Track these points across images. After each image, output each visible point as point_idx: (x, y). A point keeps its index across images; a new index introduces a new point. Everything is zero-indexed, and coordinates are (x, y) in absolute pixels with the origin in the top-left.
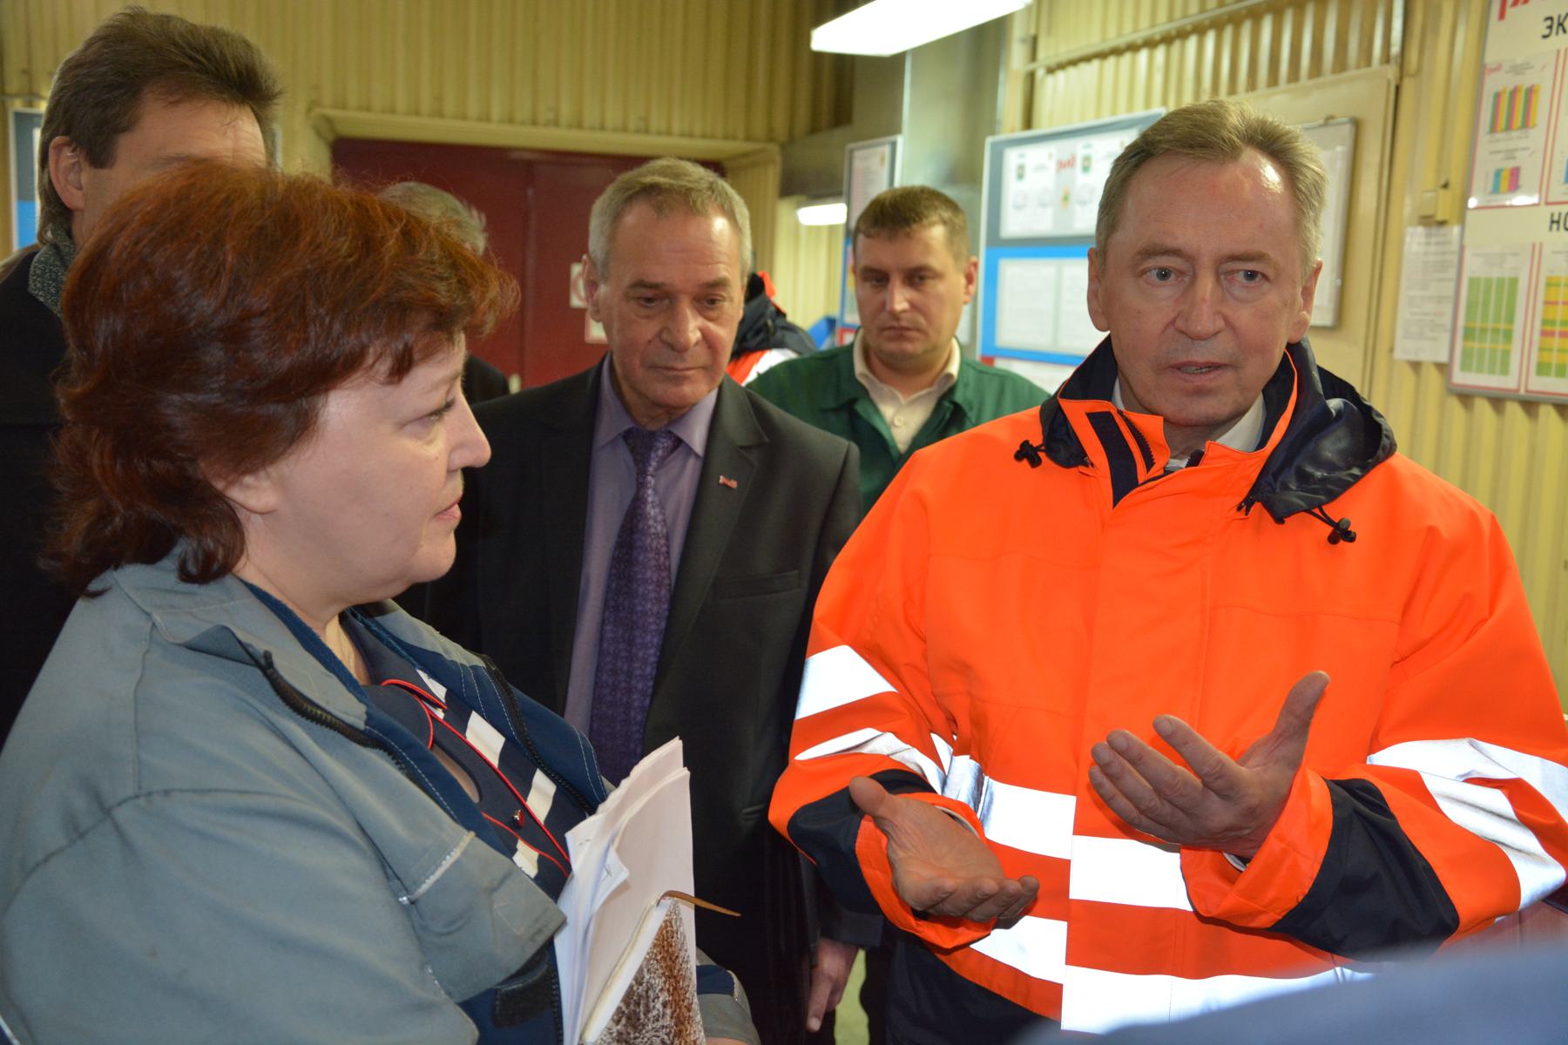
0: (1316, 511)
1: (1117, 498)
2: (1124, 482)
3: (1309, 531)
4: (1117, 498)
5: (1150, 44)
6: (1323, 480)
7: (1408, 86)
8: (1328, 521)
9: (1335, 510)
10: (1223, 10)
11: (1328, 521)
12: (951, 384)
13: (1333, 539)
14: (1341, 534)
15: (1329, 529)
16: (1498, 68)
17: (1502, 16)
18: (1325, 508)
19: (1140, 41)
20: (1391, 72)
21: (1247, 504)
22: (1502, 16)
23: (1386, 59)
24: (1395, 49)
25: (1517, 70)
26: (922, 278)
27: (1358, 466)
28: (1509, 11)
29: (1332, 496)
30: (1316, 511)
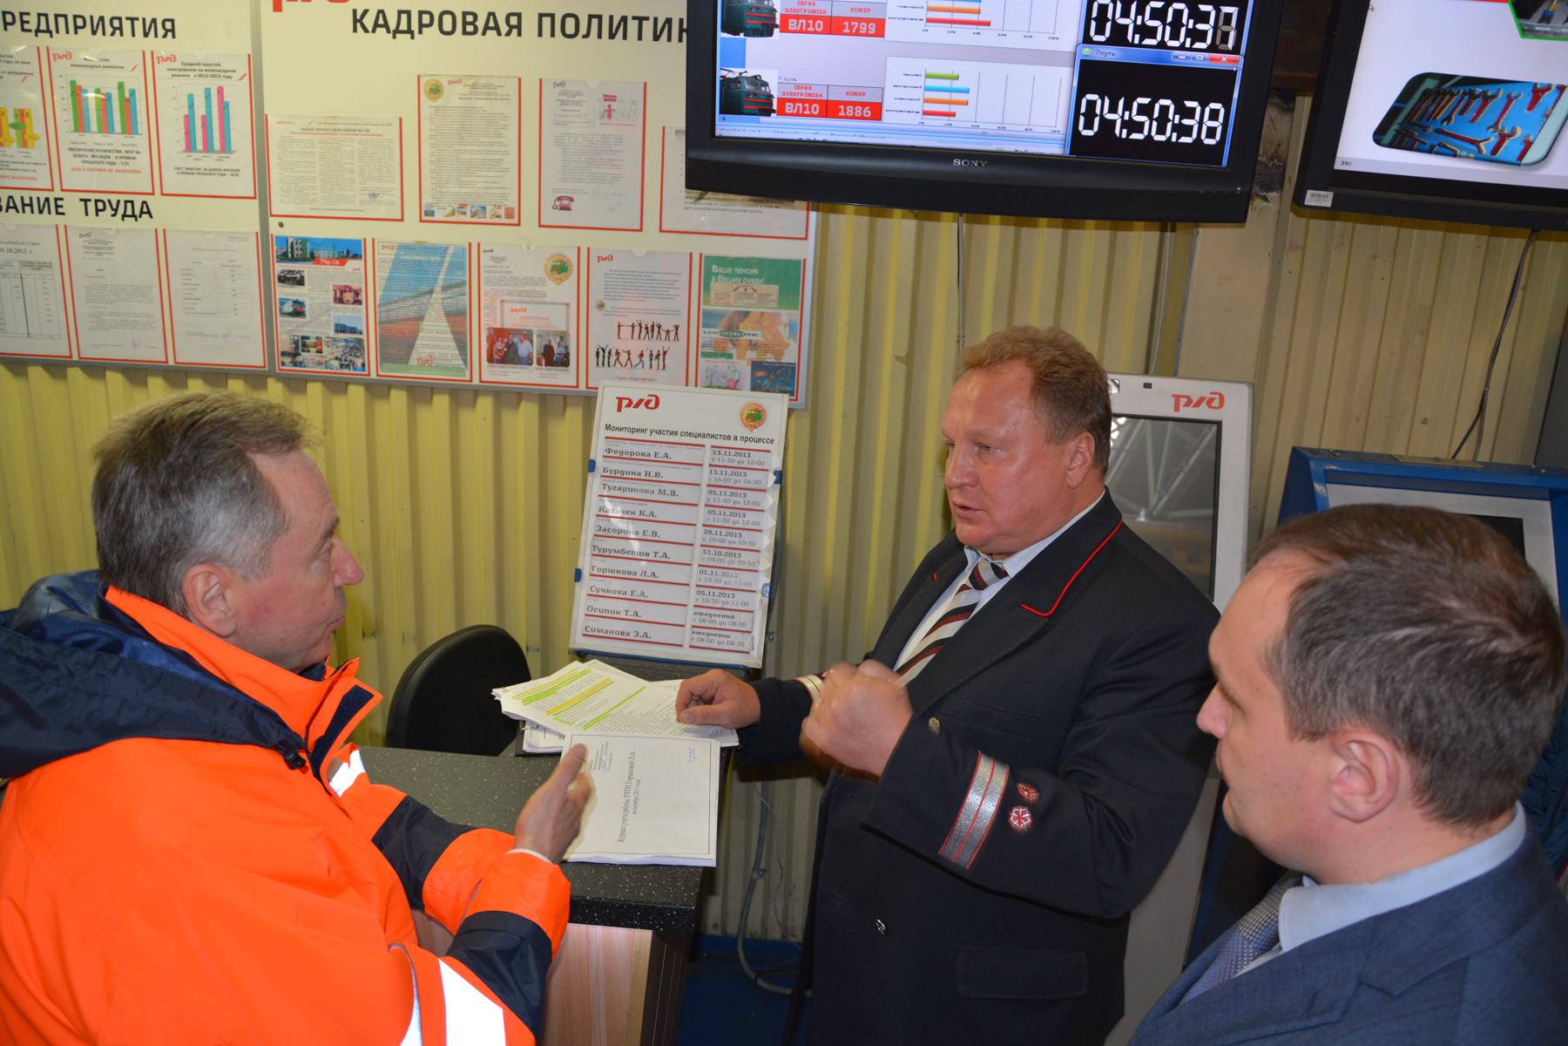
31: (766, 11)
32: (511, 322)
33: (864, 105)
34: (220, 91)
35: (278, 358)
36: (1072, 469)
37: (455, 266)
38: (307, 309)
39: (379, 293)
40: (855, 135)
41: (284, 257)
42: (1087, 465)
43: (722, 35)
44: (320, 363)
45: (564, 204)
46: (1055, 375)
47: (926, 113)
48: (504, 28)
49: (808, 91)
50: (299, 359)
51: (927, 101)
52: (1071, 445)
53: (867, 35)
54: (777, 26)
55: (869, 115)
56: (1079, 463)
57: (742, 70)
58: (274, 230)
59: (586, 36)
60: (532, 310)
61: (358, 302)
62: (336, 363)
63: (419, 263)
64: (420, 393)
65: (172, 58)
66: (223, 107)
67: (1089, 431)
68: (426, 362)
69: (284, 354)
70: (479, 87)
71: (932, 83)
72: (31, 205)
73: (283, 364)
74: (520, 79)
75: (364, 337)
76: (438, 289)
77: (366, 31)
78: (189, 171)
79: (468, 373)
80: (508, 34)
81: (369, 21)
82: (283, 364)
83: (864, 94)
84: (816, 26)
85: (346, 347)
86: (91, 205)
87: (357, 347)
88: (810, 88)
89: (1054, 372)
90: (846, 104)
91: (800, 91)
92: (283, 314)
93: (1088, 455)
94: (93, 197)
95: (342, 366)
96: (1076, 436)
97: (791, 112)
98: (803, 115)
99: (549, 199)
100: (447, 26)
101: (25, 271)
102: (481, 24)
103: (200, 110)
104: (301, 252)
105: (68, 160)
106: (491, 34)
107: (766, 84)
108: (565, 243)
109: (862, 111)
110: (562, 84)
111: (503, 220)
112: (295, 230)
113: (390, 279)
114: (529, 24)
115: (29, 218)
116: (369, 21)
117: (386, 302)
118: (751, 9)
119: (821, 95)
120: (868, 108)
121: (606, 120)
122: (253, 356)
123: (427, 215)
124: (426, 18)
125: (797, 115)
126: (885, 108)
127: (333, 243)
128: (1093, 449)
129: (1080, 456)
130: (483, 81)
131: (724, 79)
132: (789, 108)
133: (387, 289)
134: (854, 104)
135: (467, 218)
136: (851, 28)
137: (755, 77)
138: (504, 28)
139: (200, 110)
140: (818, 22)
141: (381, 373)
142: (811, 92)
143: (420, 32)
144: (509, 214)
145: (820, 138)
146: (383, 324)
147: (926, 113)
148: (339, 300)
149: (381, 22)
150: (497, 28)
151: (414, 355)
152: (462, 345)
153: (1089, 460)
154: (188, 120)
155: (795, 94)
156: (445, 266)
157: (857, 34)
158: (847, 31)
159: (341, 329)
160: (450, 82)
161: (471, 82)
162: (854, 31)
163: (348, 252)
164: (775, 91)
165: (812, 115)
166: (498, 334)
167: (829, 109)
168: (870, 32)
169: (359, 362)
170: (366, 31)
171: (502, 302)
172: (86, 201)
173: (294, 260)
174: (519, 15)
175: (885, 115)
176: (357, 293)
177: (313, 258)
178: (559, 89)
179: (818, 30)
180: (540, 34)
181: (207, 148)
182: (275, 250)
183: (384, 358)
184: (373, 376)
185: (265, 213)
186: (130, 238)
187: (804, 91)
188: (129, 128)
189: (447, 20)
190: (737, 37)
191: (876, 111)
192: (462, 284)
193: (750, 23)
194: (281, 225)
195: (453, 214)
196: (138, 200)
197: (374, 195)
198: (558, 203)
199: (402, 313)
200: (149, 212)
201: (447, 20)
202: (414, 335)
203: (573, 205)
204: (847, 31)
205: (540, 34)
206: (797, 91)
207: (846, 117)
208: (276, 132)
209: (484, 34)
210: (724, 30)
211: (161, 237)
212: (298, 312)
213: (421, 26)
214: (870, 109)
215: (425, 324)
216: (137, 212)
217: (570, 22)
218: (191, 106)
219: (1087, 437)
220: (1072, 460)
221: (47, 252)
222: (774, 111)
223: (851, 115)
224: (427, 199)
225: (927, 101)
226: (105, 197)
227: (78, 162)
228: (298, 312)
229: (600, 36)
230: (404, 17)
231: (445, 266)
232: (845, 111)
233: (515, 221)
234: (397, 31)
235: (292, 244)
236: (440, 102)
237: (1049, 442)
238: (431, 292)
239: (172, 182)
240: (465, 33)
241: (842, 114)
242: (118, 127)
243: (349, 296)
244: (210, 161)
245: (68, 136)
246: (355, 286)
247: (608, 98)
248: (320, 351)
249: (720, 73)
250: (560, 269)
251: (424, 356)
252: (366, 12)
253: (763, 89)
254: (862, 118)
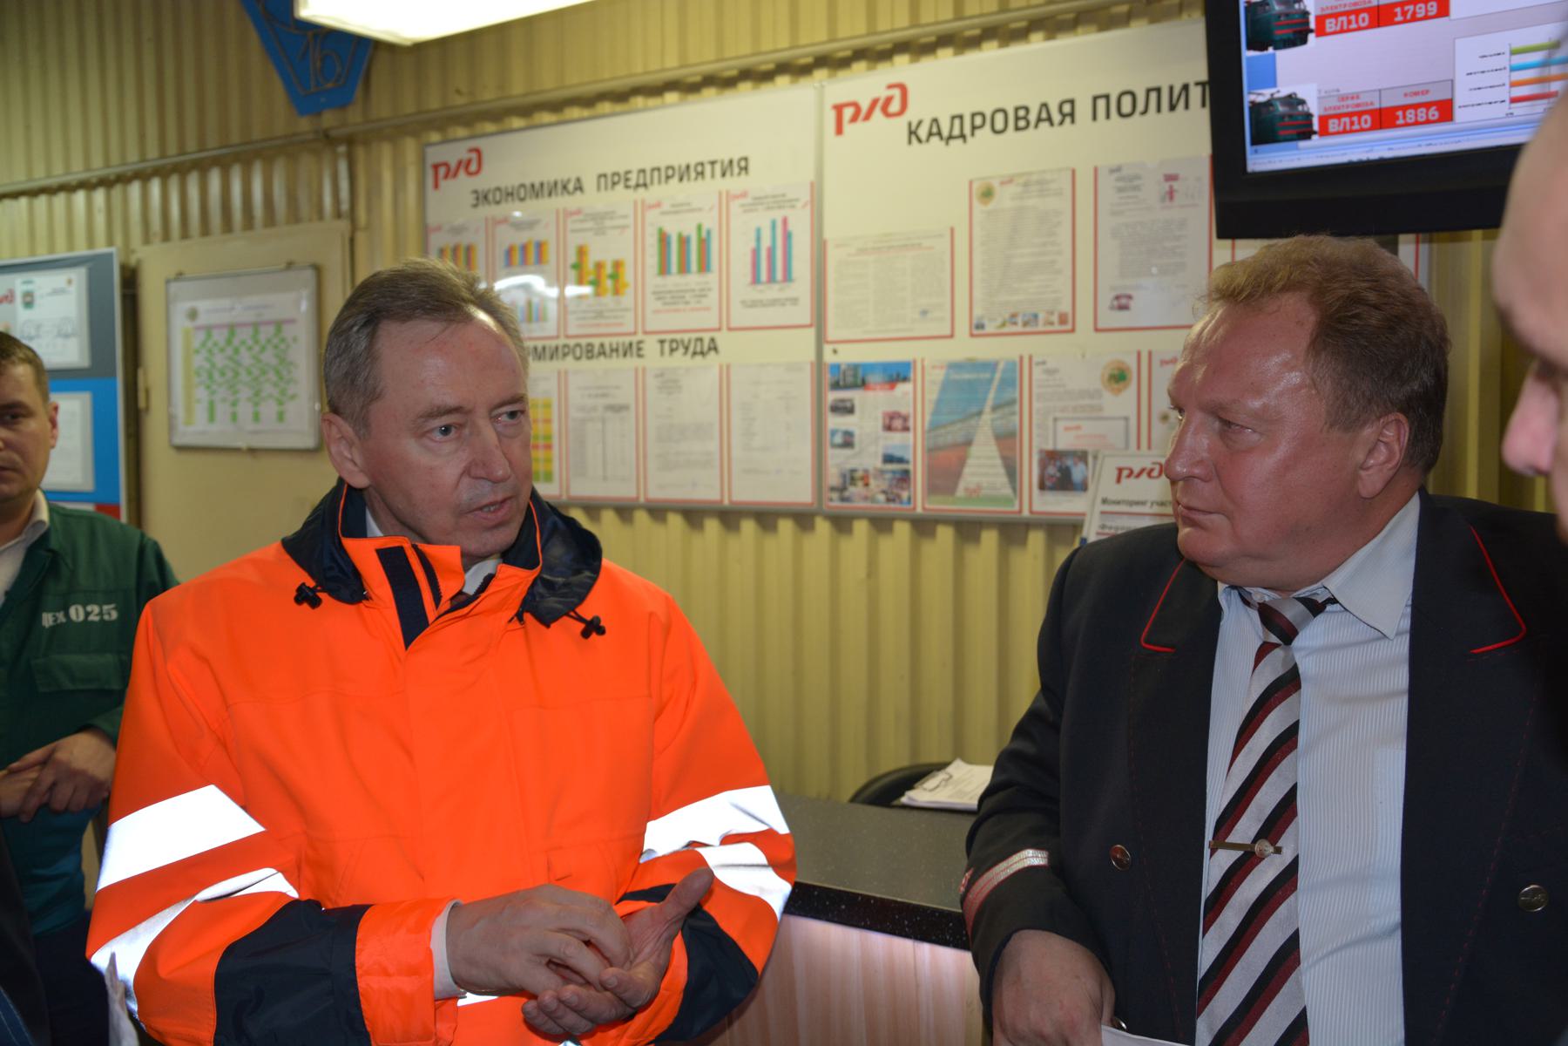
0: (572, 614)
1: (408, 640)
2: (413, 623)
3: (567, 628)
4: (408, 640)
5: (87, 186)
6: (565, 585)
7: (361, 238)
8: (580, 619)
9: (588, 610)
10: (182, 158)
11: (580, 619)
12: (43, 530)
13: (586, 634)
14: (593, 628)
15: (582, 626)
16: (439, 228)
17: (436, 186)
18: (578, 610)
19: (94, 180)
20: (344, 225)
21: (519, 617)
22: (436, 186)
23: (338, 215)
24: (345, 207)
25: (457, 230)
26: (15, 417)
27: (587, 569)
28: (442, 183)
29: (582, 598)
30: (572, 614)
31: (1297, 16)
32: (1065, 442)
33: (1427, 105)
34: (785, 221)
35: (827, 494)
36: (1368, 469)
37: (1007, 382)
38: (856, 440)
39: (928, 418)
40: (1420, 146)
41: (836, 386)
42: (1394, 463)
43: (1247, 54)
44: (866, 498)
45: (1122, 303)
46: (1355, 321)
47: (1514, 100)
48: (1056, 117)
49: (1355, 102)
50: (847, 494)
51: (1513, 85)
52: (1368, 432)
53: (1426, 18)
54: (1311, 31)
55: (1436, 117)
56: (1382, 458)
57: (1273, 90)
58: (829, 358)
59: (1145, 112)
60: (1088, 427)
61: (906, 429)
62: (882, 497)
63: (970, 382)
64: (967, 529)
65: (744, 195)
66: (787, 236)
67: (1402, 411)
68: (973, 494)
69: (833, 489)
70: (1033, 184)
71: (1518, 60)
72: (617, 350)
73: (831, 500)
74: (1074, 172)
75: (910, 467)
76: (987, 409)
77: (920, 140)
78: (754, 304)
79: (1017, 503)
80: (1061, 123)
81: (923, 132)
82: (831, 500)
83: (1427, 92)
84: (1360, 20)
85: (893, 479)
86: (667, 346)
87: (904, 478)
88: (1358, 97)
89: (1354, 316)
90: (1404, 108)
91: (1345, 103)
92: (834, 446)
93: (1396, 447)
94: (668, 337)
95: (888, 500)
96: (1379, 418)
97: (1337, 129)
98: (1351, 131)
99: (1106, 299)
100: (999, 125)
101: (609, 414)
102: (1033, 117)
103: (766, 242)
104: (856, 378)
105: (652, 304)
106: (1044, 125)
107: (1302, 102)
108: (1121, 348)
109: (1427, 114)
110: (1118, 169)
111: (1057, 327)
112: (848, 355)
113: (939, 402)
114: (1084, 109)
115: (616, 363)
116: (923, 132)
117: (935, 426)
118: (1279, 17)
119: (1372, 104)
120: (1434, 108)
121: (1168, 203)
122: (800, 492)
123: (977, 328)
124: (978, 121)
125: (1344, 132)
126: (1458, 102)
127: (885, 367)
128: (1405, 439)
129: (1383, 448)
130: (1035, 178)
131: (1255, 107)
132: (1333, 125)
133: (936, 412)
134: (1416, 107)
135: (1019, 328)
136: (1404, 13)
137: (1290, 96)
138: (1056, 117)
139: (766, 242)
140: (1361, 16)
141: (927, 506)
142: (1359, 101)
143: (973, 134)
144: (1063, 319)
145: (1374, 156)
146: (931, 451)
147: (1514, 100)
148: (888, 428)
149: (935, 131)
150: (1049, 119)
151: (962, 485)
152: (1012, 471)
153: (1398, 457)
154: (756, 253)
155: (1339, 108)
156: (996, 383)
157: (1414, 19)
158: (1399, 18)
159: (889, 459)
160: (1002, 183)
161: (1021, 180)
162: (1409, 17)
163: (897, 375)
164: (1314, 108)
165: (1362, 130)
166: (1051, 456)
167: (1384, 118)
168: (1430, 14)
169: (905, 495)
170: (920, 140)
171: (1055, 420)
172: (662, 342)
173: (847, 387)
174: (1072, 102)
175: (1459, 115)
176: (905, 419)
177: (863, 384)
178: (1116, 175)
179: (1362, 25)
180: (1095, 118)
181: (771, 279)
182: (828, 378)
183: (932, 489)
184: (919, 510)
185: (821, 340)
186: (701, 376)
187: (1350, 102)
188: (704, 267)
189: (999, 118)
190: (1265, 52)
191: (1445, 110)
192: (1011, 403)
193: (1280, 33)
194: (835, 352)
195: (1003, 325)
196: (706, 337)
197: (924, 313)
198: (1116, 303)
199: (949, 439)
200: (715, 349)
201: (999, 118)
202: (962, 461)
203: (1132, 304)
204: (1399, 18)
205: (1095, 118)
206: (1342, 103)
207: (1407, 125)
208: (833, 257)
209: (1036, 126)
210: (1250, 47)
211: (725, 373)
212: (848, 442)
213: (974, 128)
214: (1437, 109)
215: (974, 450)
216: (706, 348)
217: (1127, 101)
218: (758, 239)
219: (1398, 421)
220: (1370, 452)
221: (626, 395)
222: (1315, 133)
223: (1413, 120)
224: (978, 311)
225: (1513, 85)
226: (678, 337)
227: (659, 305)
228: (848, 442)
229: (1159, 110)
230: (957, 122)
231: (996, 383)
232: (1404, 117)
233: (1069, 327)
234: (950, 137)
235: (844, 373)
236: (992, 206)
237: (1331, 426)
238: (980, 413)
239: (740, 316)
240: (1017, 129)
241: (1401, 121)
242: (694, 265)
243: (898, 423)
244: (773, 292)
245: (654, 280)
246: (903, 411)
247: (1171, 178)
248: (867, 485)
249: (1248, 98)
250: (1118, 377)
251: (972, 486)
252: (920, 123)
253: (1300, 108)
254: (1428, 122)
